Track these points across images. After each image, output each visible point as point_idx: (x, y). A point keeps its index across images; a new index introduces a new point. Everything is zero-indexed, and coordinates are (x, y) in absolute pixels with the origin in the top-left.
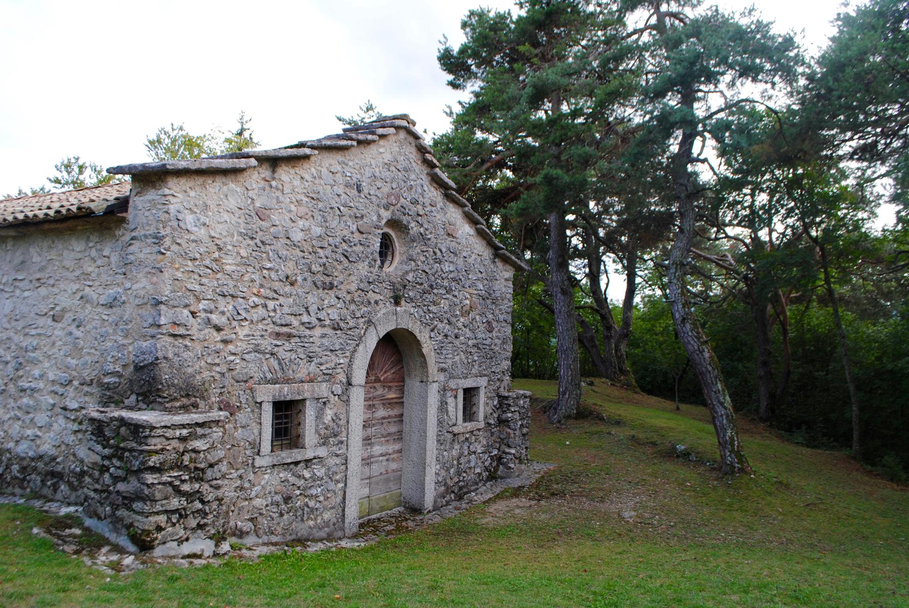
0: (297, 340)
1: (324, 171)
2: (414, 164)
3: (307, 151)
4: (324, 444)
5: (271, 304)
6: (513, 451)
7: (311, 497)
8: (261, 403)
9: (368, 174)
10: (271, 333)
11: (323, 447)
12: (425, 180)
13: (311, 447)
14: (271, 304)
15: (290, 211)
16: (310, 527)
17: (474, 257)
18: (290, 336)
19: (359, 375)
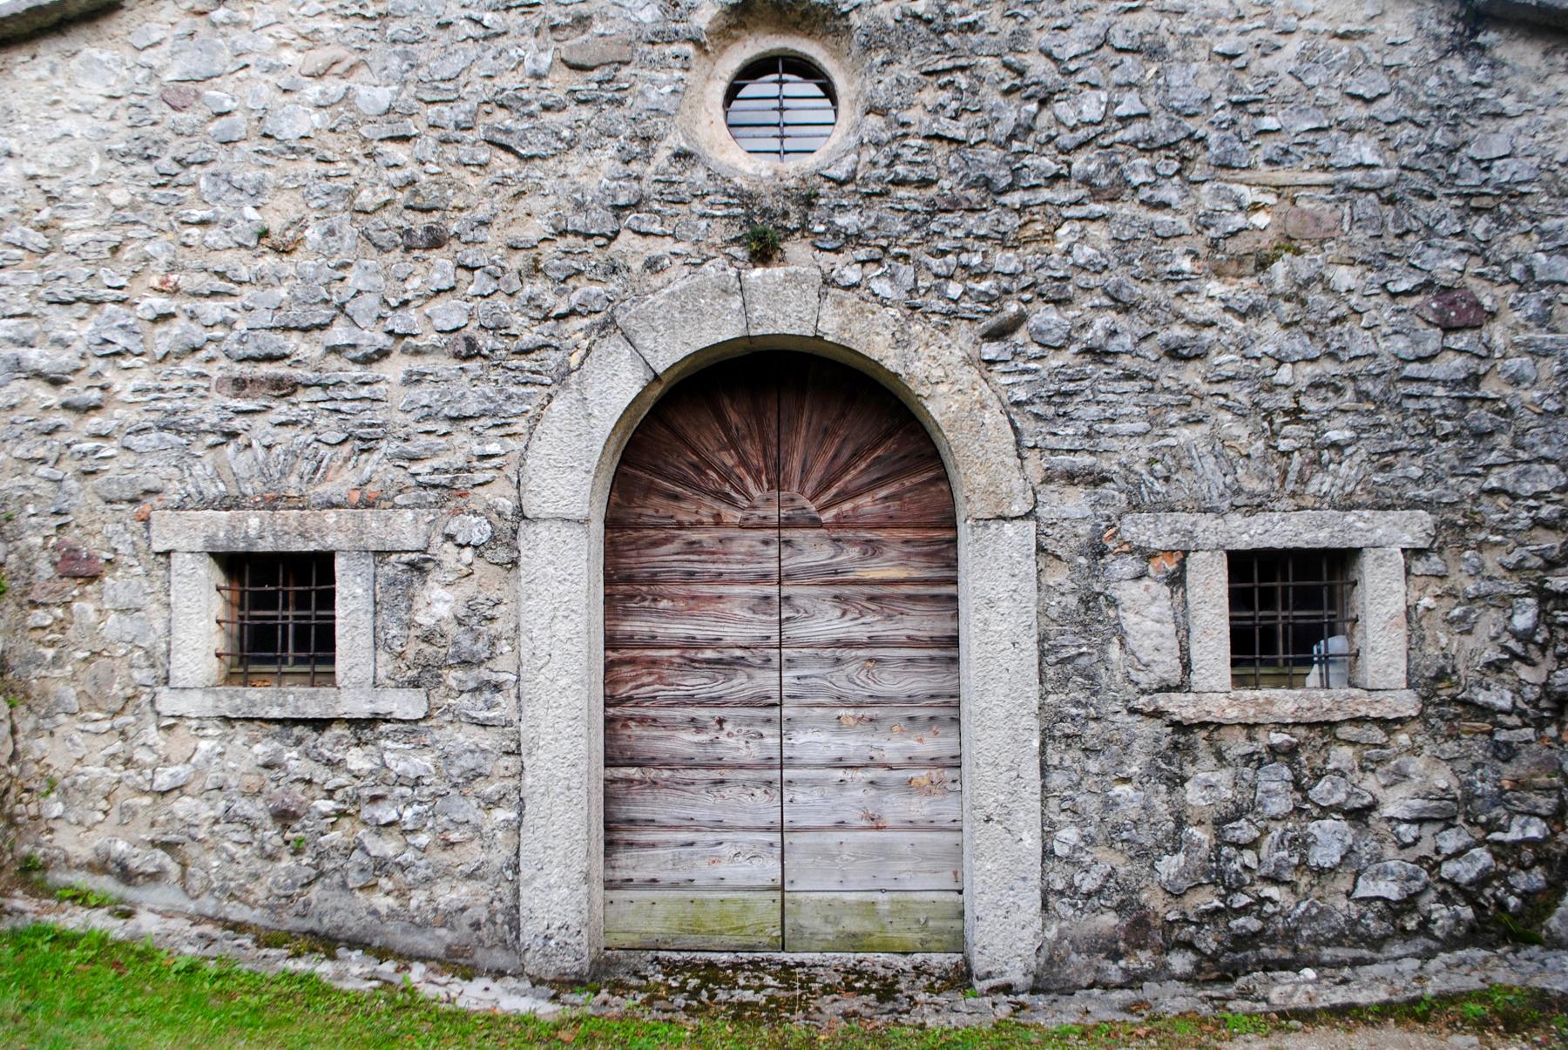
0: (317, 394)
4: (415, 684)
5: (213, 310)
8: (167, 554)
10: (220, 383)
11: (410, 693)
13: (359, 685)
16: (375, 912)
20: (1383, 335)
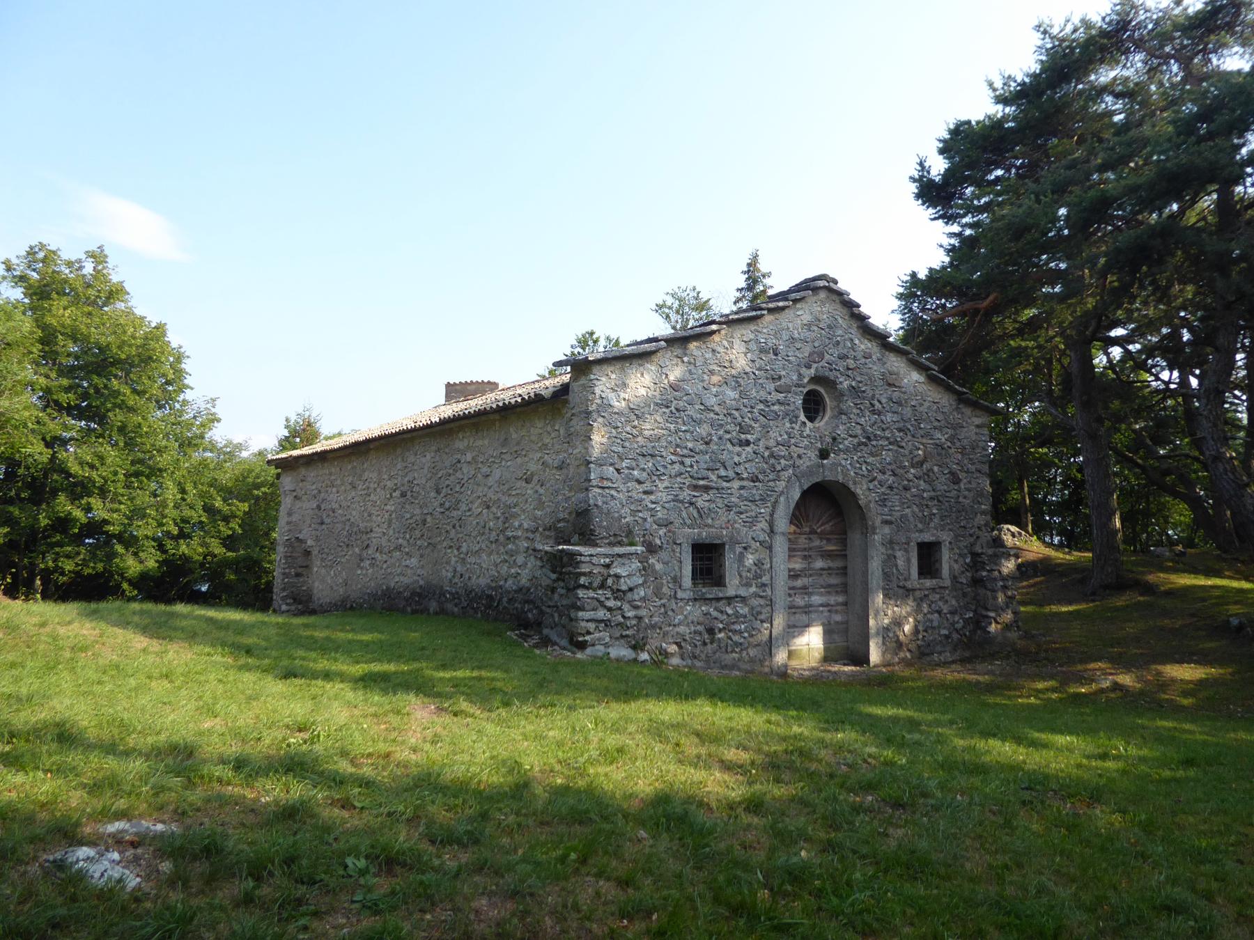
2: (840, 321)
3: (714, 327)
5: (688, 461)
7: (735, 632)
9: (785, 337)
12: (855, 333)
14: (688, 461)
15: (703, 381)
17: (926, 404)
18: (707, 489)
20: (942, 484)
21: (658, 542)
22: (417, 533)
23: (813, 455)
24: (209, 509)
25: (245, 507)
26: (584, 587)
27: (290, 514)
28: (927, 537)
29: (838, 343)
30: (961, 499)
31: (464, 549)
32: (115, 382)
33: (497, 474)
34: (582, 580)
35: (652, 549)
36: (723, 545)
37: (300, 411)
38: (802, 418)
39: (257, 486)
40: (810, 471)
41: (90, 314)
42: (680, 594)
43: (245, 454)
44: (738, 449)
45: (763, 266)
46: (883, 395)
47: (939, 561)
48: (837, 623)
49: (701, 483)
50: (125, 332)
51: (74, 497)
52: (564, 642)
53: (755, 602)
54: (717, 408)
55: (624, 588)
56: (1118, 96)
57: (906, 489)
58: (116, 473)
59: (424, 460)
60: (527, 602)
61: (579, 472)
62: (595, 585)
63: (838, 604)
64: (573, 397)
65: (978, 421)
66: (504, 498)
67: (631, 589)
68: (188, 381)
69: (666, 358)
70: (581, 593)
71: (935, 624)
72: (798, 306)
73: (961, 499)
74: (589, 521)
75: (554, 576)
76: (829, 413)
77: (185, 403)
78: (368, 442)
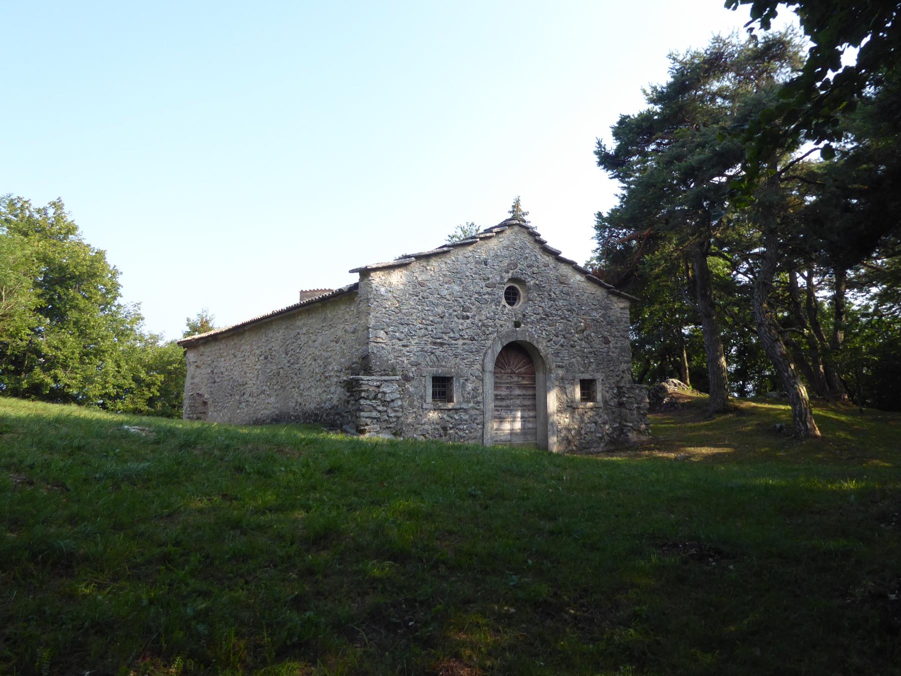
1: (460, 257)
5: (430, 328)
6: (631, 424)
9: (492, 255)
18: (442, 344)
19: (490, 366)
20: (597, 344)
21: (411, 375)
22: (274, 381)
23: (510, 325)
24: (136, 379)
25: (161, 377)
26: (363, 398)
27: (193, 378)
28: (587, 376)
29: (527, 258)
30: (610, 354)
31: (301, 388)
32: (71, 291)
33: (320, 339)
34: (363, 394)
35: (407, 379)
36: (452, 378)
37: (200, 312)
38: (504, 302)
39: (170, 363)
40: (508, 335)
41: (54, 245)
42: (425, 406)
43: (161, 343)
44: (461, 321)
45: (523, 208)
46: (557, 289)
47: (595, 391)
48: (529, 428)
49: (438, 341)
50: (78, 256)
51: (46, 370)
52: (353, 431)
53: (473, 412)
54: (448, 297)
55: (388, 399)
56: (725, 98)
57: (573, 346)
58: (73, 353)
59: (278, 335)
60: (338, 414)
61: (363, 336)
62: (371, 397)
63: (530, 417)
64: (360, 291)
65: (622, 305)
66: (324, 354)
67: (392, 401)
68: (121, 291)
69: (416, 266)
70: (362, 402)
71: (593, 430)
72: (500, 235)
73: (610, 354)
74: (369, 362)
75: (348, 394)
76: (522, 300)
77: (119, 306)
78: (244, 325)
